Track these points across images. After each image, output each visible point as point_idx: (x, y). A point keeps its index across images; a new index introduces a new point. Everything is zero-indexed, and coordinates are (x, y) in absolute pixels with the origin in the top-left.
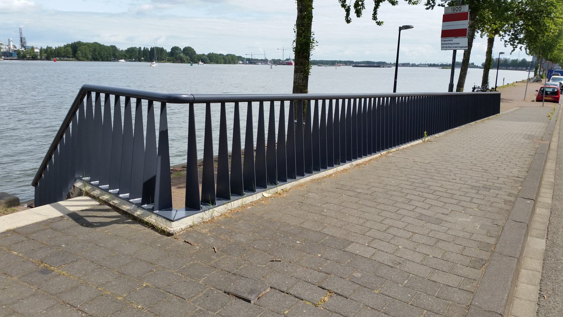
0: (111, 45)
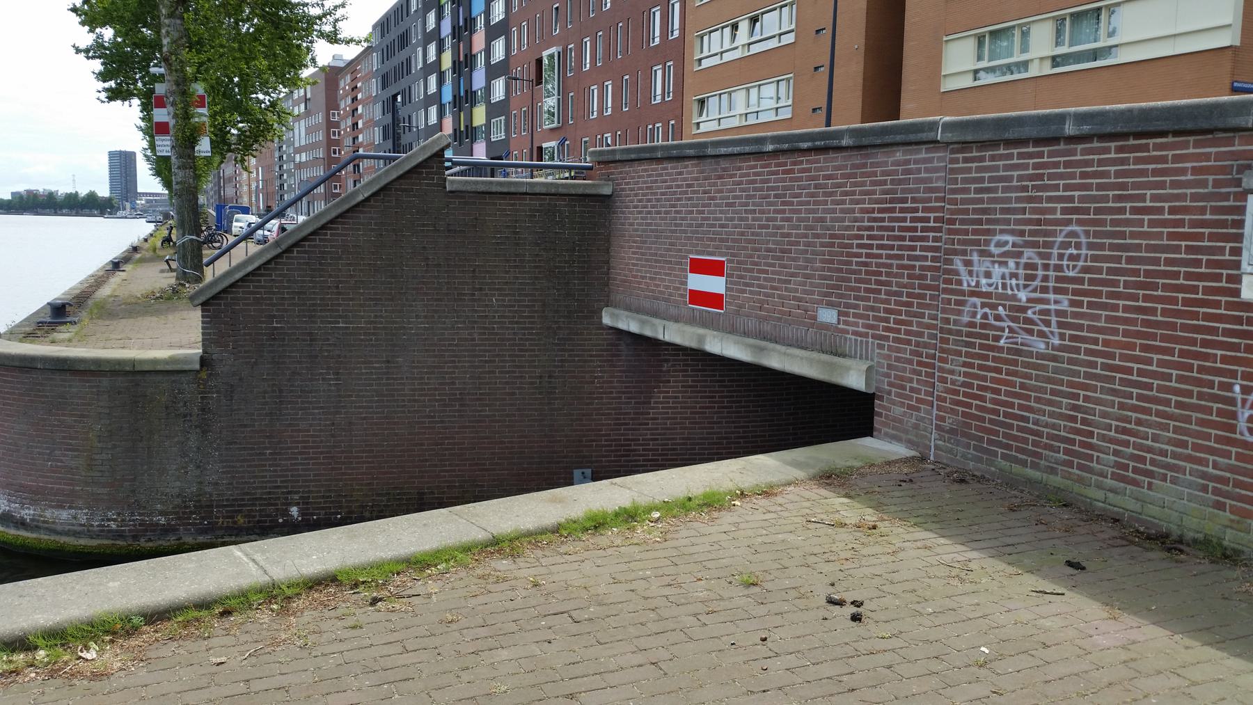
0: (27, 188)
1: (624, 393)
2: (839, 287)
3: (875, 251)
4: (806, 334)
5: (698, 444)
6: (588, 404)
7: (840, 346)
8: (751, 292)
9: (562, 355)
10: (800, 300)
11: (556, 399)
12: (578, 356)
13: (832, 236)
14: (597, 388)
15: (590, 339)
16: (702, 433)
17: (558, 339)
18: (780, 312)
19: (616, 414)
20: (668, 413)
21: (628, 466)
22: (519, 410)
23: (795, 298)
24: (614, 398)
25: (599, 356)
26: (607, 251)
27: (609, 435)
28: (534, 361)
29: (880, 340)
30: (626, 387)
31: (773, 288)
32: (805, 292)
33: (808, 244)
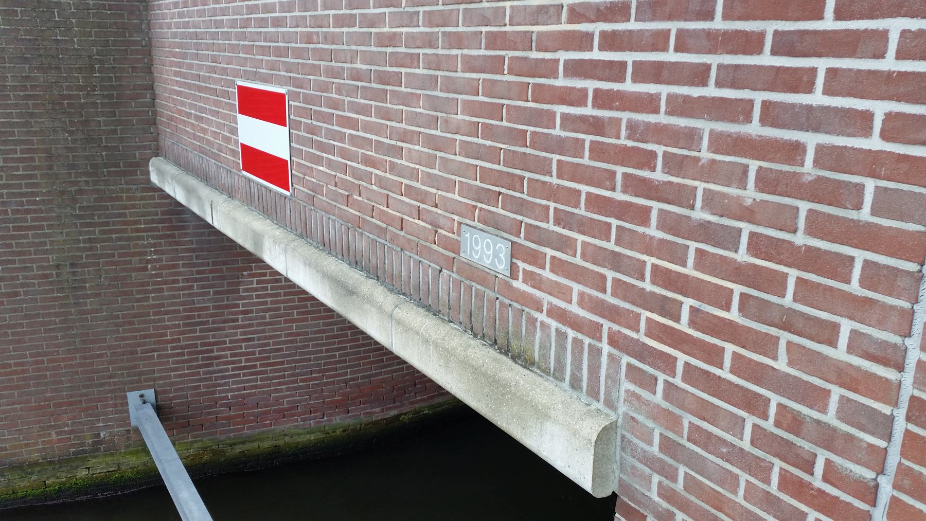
1: (196, 280)
2: (515, 182)
3: (629, 86)
4: (436, 280)
5: (311, 340)
6: (138, 300)
7: (518, 335)
8: (330, 164)
9: (89, 233)
10: (422, 197)
11: (87, 296)
12: (116, 231)
13: (494, 41)
14: (152, 276)
15: (134, 206)
16: (317, 325)
17: (80, 207)
18: (383, 216)
19: (185, 310)
20: (266, 303)
21: (210, 379)
22: (26, 317)
23: (410, 192)
24: (179, 289)
25: (150, 230)
26: (149, 69)
27: (179, 340)
28: (45, 243)
29: (641, 359)
30: (198, 272)
31: (368, 161)
32: (431, 180)
33: (436, 63)
